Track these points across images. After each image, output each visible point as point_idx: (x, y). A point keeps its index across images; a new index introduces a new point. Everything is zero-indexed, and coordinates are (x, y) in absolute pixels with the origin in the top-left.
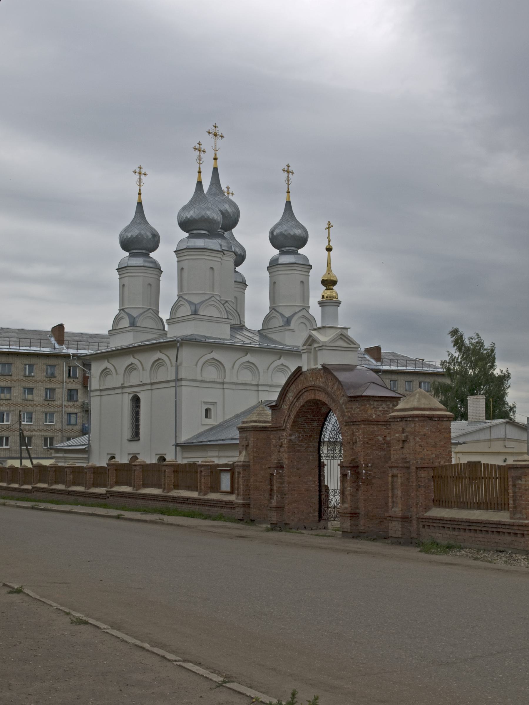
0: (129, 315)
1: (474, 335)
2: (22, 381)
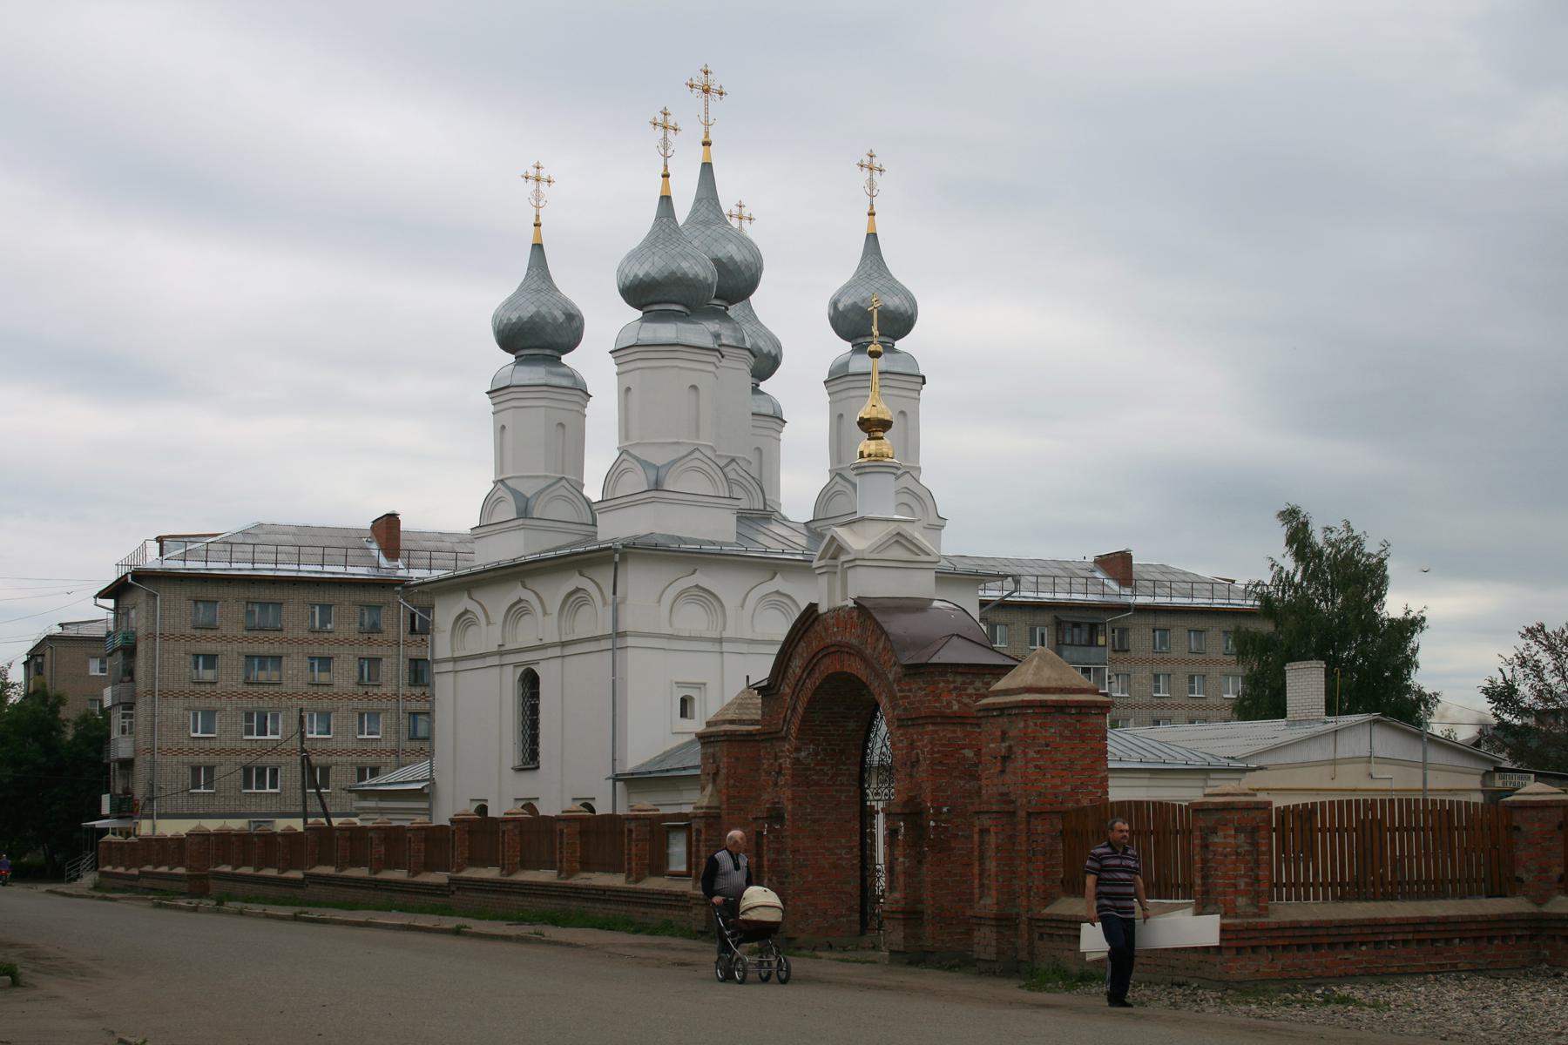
0: (514, 492)
1: (1340, 526)
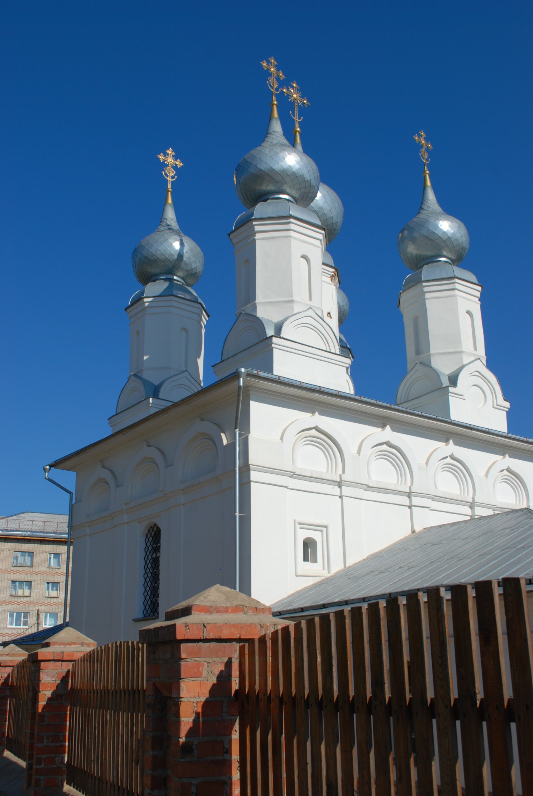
2: (46, 573)
